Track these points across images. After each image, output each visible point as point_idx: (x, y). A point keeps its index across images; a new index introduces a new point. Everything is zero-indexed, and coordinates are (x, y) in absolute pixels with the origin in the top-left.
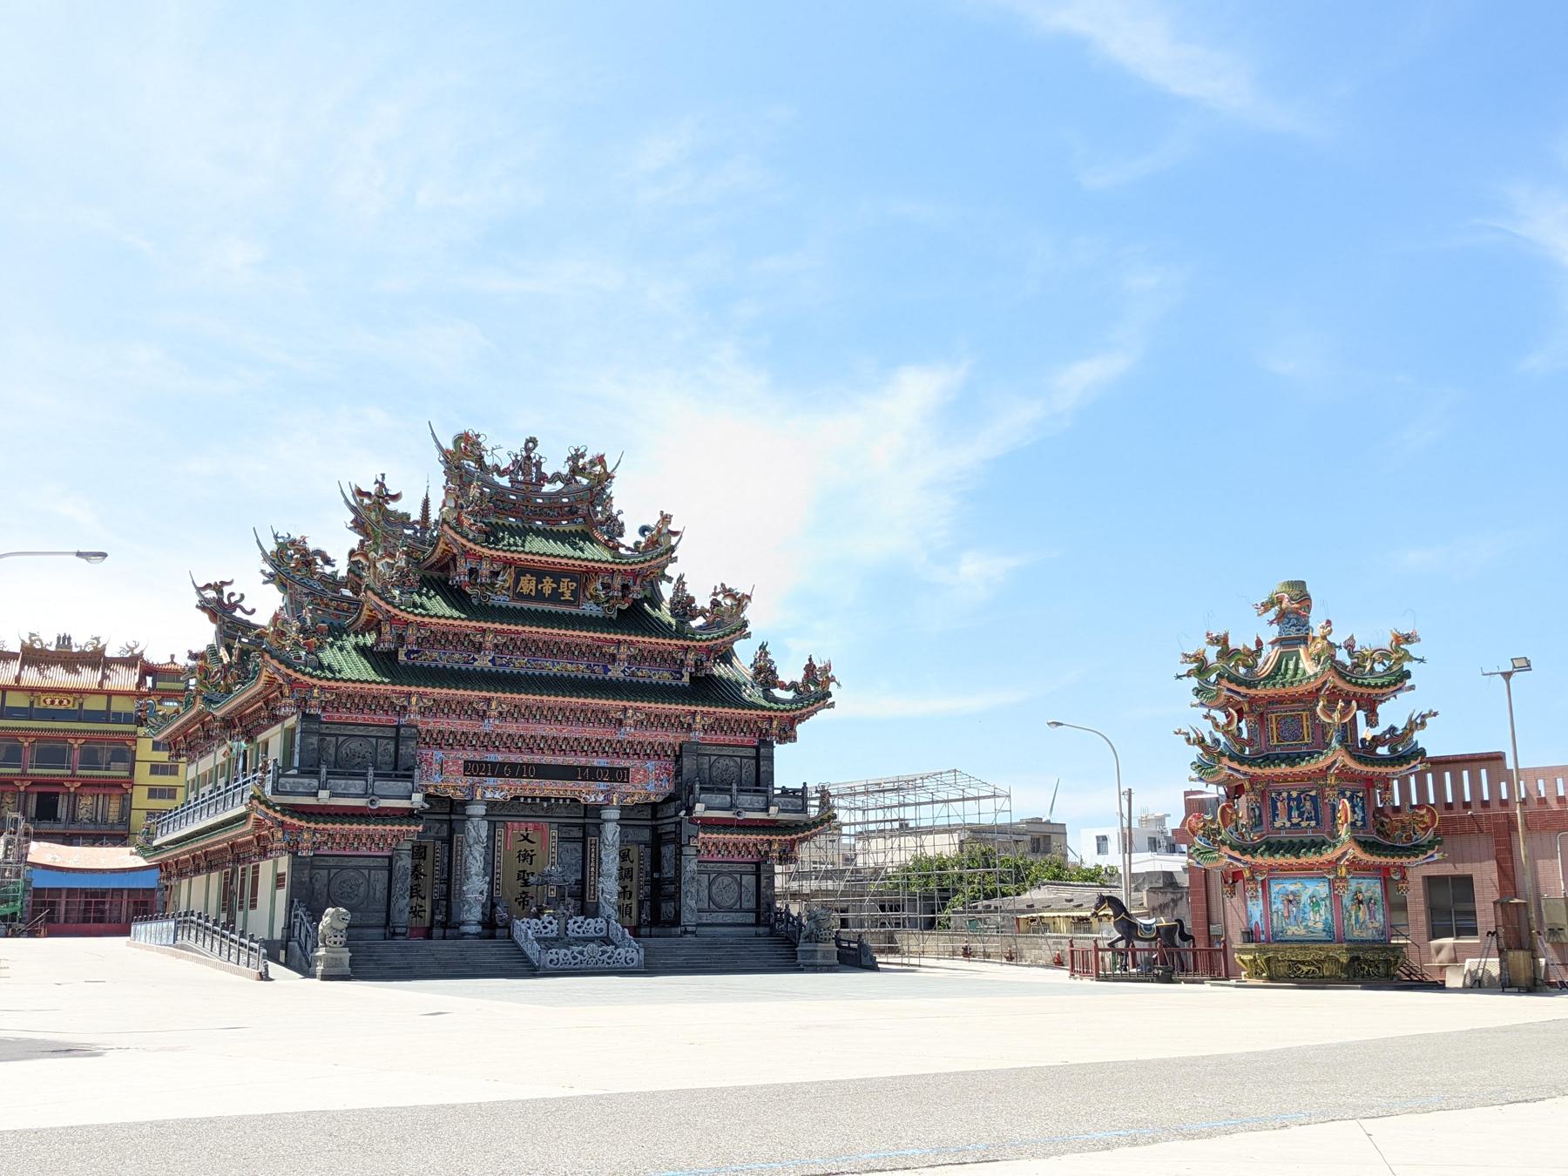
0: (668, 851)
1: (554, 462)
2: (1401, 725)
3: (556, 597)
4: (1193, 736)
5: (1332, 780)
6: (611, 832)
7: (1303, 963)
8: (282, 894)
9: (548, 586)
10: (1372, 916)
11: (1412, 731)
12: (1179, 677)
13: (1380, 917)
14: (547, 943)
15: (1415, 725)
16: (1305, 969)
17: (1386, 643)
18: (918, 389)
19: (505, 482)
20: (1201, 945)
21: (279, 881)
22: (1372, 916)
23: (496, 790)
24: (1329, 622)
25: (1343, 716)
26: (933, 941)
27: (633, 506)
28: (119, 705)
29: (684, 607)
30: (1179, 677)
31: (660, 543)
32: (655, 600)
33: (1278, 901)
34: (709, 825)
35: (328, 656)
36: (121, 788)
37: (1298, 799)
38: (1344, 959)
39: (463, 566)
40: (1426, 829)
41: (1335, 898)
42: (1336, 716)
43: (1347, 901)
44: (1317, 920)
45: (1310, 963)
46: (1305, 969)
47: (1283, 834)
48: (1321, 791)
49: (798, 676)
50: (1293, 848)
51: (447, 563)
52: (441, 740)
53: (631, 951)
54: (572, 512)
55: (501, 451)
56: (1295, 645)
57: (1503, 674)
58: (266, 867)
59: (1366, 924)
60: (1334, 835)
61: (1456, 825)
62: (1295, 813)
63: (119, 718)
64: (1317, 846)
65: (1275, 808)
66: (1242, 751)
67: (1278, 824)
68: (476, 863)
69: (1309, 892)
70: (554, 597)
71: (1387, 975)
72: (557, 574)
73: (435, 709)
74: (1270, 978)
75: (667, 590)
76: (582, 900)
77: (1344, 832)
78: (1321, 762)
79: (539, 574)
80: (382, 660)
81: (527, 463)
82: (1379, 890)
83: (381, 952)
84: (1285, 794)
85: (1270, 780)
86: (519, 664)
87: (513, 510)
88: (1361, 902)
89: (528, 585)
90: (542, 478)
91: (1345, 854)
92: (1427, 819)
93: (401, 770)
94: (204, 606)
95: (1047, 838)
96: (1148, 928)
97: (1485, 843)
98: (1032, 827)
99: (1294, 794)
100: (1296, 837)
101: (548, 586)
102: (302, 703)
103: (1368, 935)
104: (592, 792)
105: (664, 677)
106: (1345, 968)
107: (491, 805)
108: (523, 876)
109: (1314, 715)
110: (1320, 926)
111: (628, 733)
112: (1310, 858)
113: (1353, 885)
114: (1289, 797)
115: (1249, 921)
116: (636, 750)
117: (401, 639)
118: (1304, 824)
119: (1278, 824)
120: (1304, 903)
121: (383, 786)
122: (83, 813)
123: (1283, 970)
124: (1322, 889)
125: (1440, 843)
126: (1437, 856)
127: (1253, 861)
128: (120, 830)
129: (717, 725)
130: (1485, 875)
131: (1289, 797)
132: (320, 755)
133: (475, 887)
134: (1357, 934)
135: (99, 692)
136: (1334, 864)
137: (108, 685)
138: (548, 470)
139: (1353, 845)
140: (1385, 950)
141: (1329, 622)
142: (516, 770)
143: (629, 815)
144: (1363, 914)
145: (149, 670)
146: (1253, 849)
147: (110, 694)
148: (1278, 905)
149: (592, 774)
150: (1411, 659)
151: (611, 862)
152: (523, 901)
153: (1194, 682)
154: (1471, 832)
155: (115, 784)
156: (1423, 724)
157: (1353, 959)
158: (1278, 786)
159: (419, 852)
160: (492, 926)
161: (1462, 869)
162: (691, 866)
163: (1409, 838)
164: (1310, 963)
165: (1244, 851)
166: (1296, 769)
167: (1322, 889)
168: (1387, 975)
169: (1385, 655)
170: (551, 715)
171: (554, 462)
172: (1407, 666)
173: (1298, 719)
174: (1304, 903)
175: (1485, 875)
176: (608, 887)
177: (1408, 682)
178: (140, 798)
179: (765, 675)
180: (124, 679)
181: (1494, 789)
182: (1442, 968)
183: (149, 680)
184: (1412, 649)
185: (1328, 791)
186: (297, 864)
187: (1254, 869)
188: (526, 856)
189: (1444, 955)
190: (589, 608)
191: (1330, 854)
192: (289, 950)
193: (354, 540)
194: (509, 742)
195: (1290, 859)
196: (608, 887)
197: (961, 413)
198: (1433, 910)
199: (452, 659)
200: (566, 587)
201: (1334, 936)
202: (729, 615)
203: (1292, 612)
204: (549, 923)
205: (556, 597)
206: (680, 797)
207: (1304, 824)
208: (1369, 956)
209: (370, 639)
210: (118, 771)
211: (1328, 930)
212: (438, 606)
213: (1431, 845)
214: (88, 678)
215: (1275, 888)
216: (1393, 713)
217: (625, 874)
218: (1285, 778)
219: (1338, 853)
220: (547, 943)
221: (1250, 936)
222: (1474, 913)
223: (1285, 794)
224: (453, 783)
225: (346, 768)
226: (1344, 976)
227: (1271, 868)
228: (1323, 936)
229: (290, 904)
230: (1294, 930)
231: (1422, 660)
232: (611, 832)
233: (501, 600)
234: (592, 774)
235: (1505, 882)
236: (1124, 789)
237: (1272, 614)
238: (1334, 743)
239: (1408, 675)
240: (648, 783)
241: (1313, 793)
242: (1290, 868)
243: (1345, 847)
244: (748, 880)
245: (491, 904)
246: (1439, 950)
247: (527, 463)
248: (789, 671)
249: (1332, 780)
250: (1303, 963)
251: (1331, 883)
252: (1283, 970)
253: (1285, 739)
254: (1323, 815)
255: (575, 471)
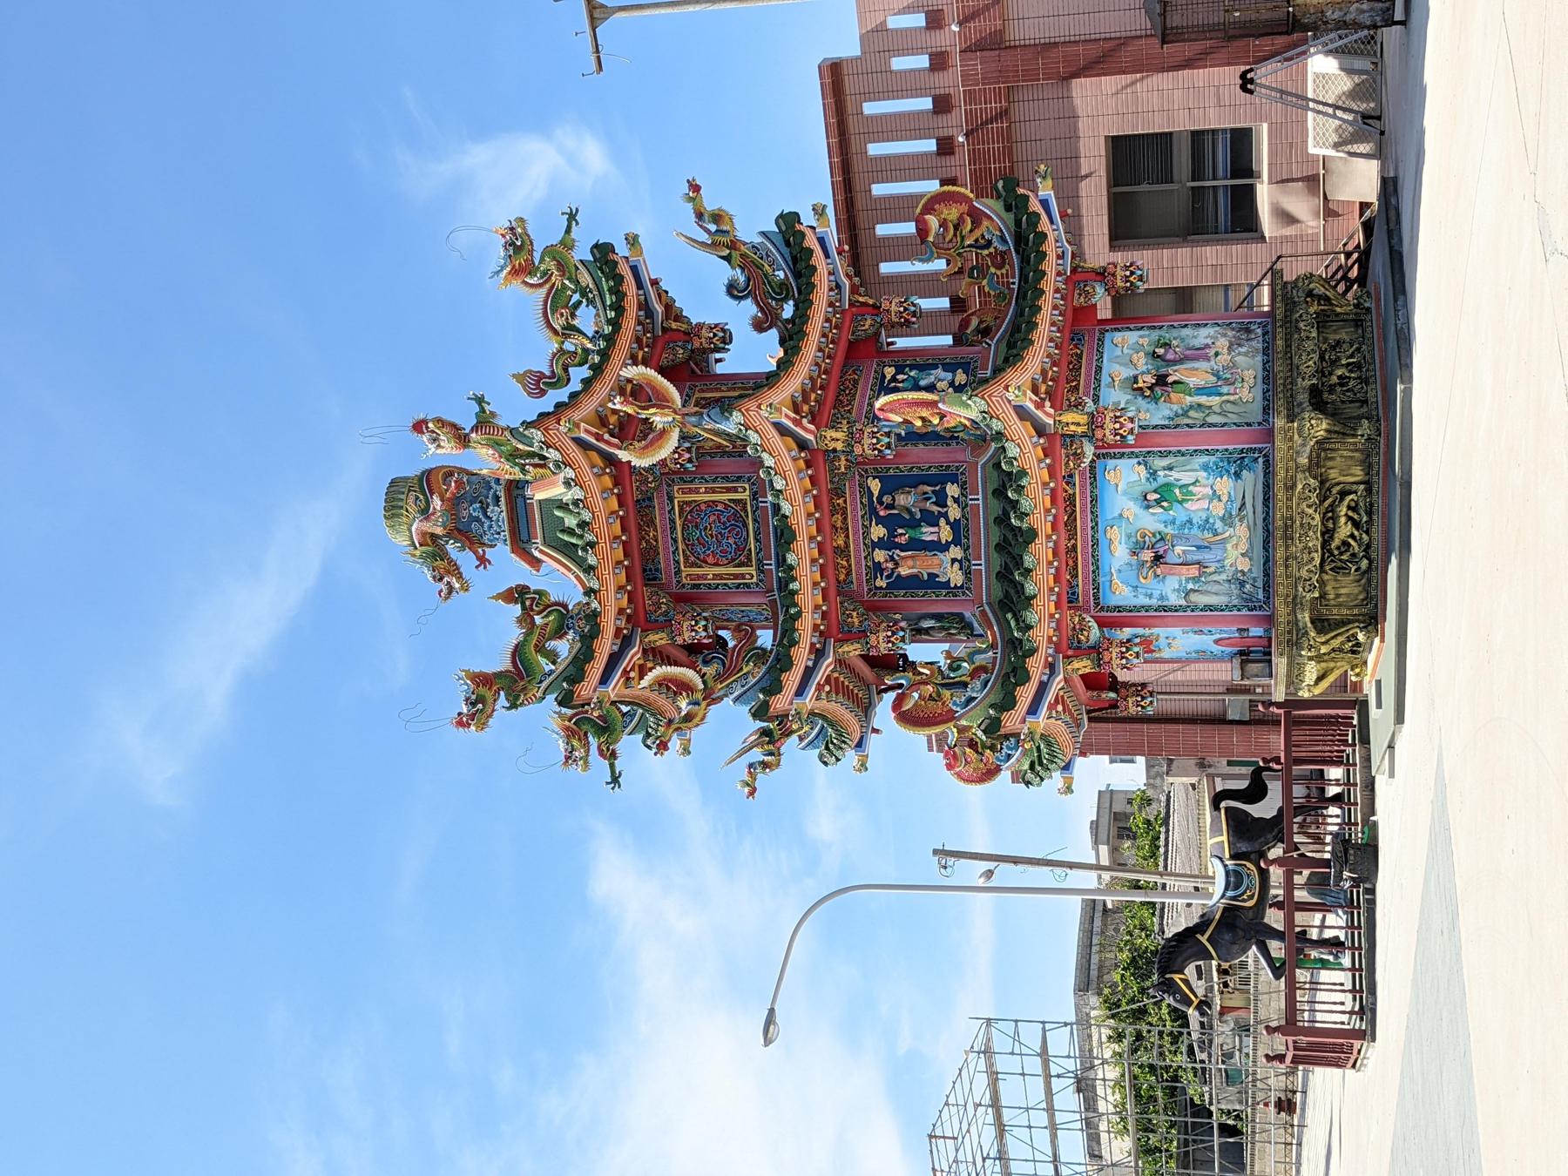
2: (727, 273)
4: (757, 755)
5: (835, 438)
7: (1328, 534)
10: (1199, 353)
11: (733, 245)
12: (615, 780)
13: (1203, 336)
15: (724, 243)
16: (1344, 530)
17: (528, 299)
20: (1277, 742)
22: (1199, 353)
24: (419, 427)
25: (661, 402)
30: (615, 780)
33: (1157, 588)
37: (891, 523)
38: (1320, 427)
40: (977, 217)
41: (1145, 446)
42: (659, 419)
43: (1156, 414)
44: (1210, 493)
45: (1330, 516)
46: (1344, 530)
47: (980, 565)
48: (864, 467)
50: (1012, 543)
56: (527, 507)
57: (594, 23)
59: (1224, 370)
60: (981, 437)
61: (992, 160)
62: (927, 533)
64: (1006, 482)
65: (913, 582)
66: (762, 655)
67: (956, 577)
69: (1132, 509)
71: (1358, 323)
74: (1373, 621)
77: (964, 411)
78: (779, 459)
82: (1132, 337)
84: (880, 555)
85: (838, 588)
88: (1161, 380)
91: (1021, 412)
92: (952, 213)
95: (1117, 816)
96: (1234, 880)
97: (1032, 109)
98: (1103, 835)
99: (878, 532)
100: (984, 535)
103: (1249, 364)
106: (1344, 425)
109: (667, 474)
110: (1225, 485)
112: (1036, 503)
113: (1114, 396)
114: (887, 544)
115: (1215, 659)
118: (954, 512)
119: (956, 577)
120: (1167, 527)
123: (1346, 588)
124: (1124, 477)
125: (1012, 183)
126: (1046, 190)
127: (1044, 651)
130: (1105, 107)
131: (887, 544)
134: (1248, 393)
136: (1054, 442)
139: (996, 389)
140: (1290, 325)
141: (419, 427)
144: (1195, 375)
146: (1017, 650)
148: (1170, 589)
150: (567, 244)
153: (630, 745)
154: (1007, 136)
156: (717, 218)
157: (1318, 402)
158: (859, 567)
161: (1094, 159)
163: (1001, 259)
164: (1330, 516)
165: (1015, 674)
166: (803, 527)
167: (1124, 477)
168: (1358, 323)
169: (555, 301)
172: (582, 252)
173: (692, 514)
174: (1167, 527)
175: (1105, 107)
177: (622, 250)
181: (905, 85)
182: (1330, 213)
184: (544, 236)
185: (865, 448)
187: (1071, 646)
189: (1301, 205)
191: (1023, 449)
195: (1040, 555)
201: (1253, 453)
207: (954, 512)
208: (1309, 364)
211: (1237, 464)
213: (1016, 205)
215: (1121, 593)
216: (702, 291)
218: (832, 556)
219: (1019, 430)
221: (1252, 655)
222: (1197, 136)
223: (880, 555)
226: (1365, 428)
227: (1070, 600)
228: (1251, 480)
230: (1237, 551)
231: (572, 217)
235: (1125, 56)
236: (930, 871)
237: (465, 559)
238: (732, 425)
239: (603, 252)
241: (875, 486)
242: (1067, 556)
243: (1009, 405)
246: (1287, 218)
249: (835, 438)
250: (1328, 534)
251: (1106, 452)
252: (1346, 588)
253: (741, 548)
254: (925, 474)
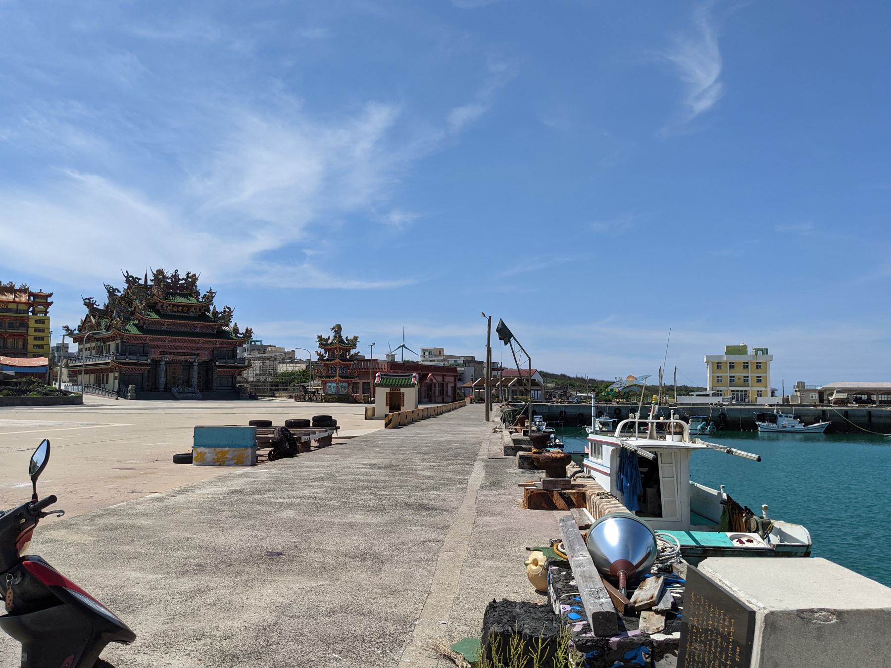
0: (210, 372)
1: (182, 275)
3: (182, 311)
6: (196, 368)
8: (117, 382)
9: (180, 309)
14: (179, 393)
18: (379, 117)
19: (169, 281)
21: (116, 378)
23: (167, 358)
26: (283, 394)
27: (202, 286)
28: (21, 307)
29: (215, 313)
31: (210, 297)
32: (209, 311)
34: (220, 367)
35: (128, 327)
36: (24, 337)
39: (159, 305)
44: (334, 390)
49: (244, 331)
51: (156, 303)
52: (153, 347)
53: (200, 395)
54: (187, 288)
55: (169, 273)
58: (111, 376)
59: (343, 391)
63: (21, 312)
64: (333, 377)
68: (163, 375)
70: (182, 312)
72: (183, 306)
73: (153, 339)
75: (211, 308)
76: (188, 383)
79: (178, 306)
80: (139, 327)
81: (175, 276)
83: (143, 393)
86: (173, 328)
87: (171, 288)
89: (175, 309)
90: (179, 279)
93: (145, 354)
94: (85, 304)
101: (180, 309)
102: (122, 339)
104: (191, 359)
105: (209, 331)
107: (166, 362)
108: (174, 378)
111: (200, 345)
116: (202, 349)
117: (144, 323)
121: (141, 358)
122: (9, 345)
128: (24, 351)
129: (222, 343)
132: (125, 350)
133: (162, 380)
135: (14, 302)
137: (17, 300)
138: (181, 277)
142: (171, 353)
143: (200, 364)
145: (31, 294)
147: (18, 303)
149: (193, 354)
151: (196, 375)
152: (174, 383)
155: (21, 335)
159: (149, 372)
160: (166, 389)
162: (215, 376)
170: (181, 341)
171: (182, 275)
176: (195, 381)
178: (30, 340)
179: (236, 330)
180: (23, 298)
183: (32, 298)
186: (120, 375)
188: (174, 373)
190: (191, 314)
192: (121, 393)
193: (126, 286)
194: (170, 347)
196: (195, 381)
197: (395, 135)
198: (363, 389)
199: (158, 328)
200: (185, 309)
201: (337, 393)
202: (228, 314)
203: (338, 329)
204: (180, 389)
205: (182, 311)
206: (213, 360)
209: (137, 322)
210: (22, 330)
212: (154, 316)
214: (9, 297)
216: (353, 352)
217: (199, 377)
220: (179, 393)
224: (157, 356)
225: (132, 354)
229: (119, 384)
232: (196, 368)
233: (169, 313)
234: (193, 354)
240: (205, 357)
244: (230, 380)
245: (166, 384)
247: (175, 276)
248: (242, 330)
255: (188, 277)
